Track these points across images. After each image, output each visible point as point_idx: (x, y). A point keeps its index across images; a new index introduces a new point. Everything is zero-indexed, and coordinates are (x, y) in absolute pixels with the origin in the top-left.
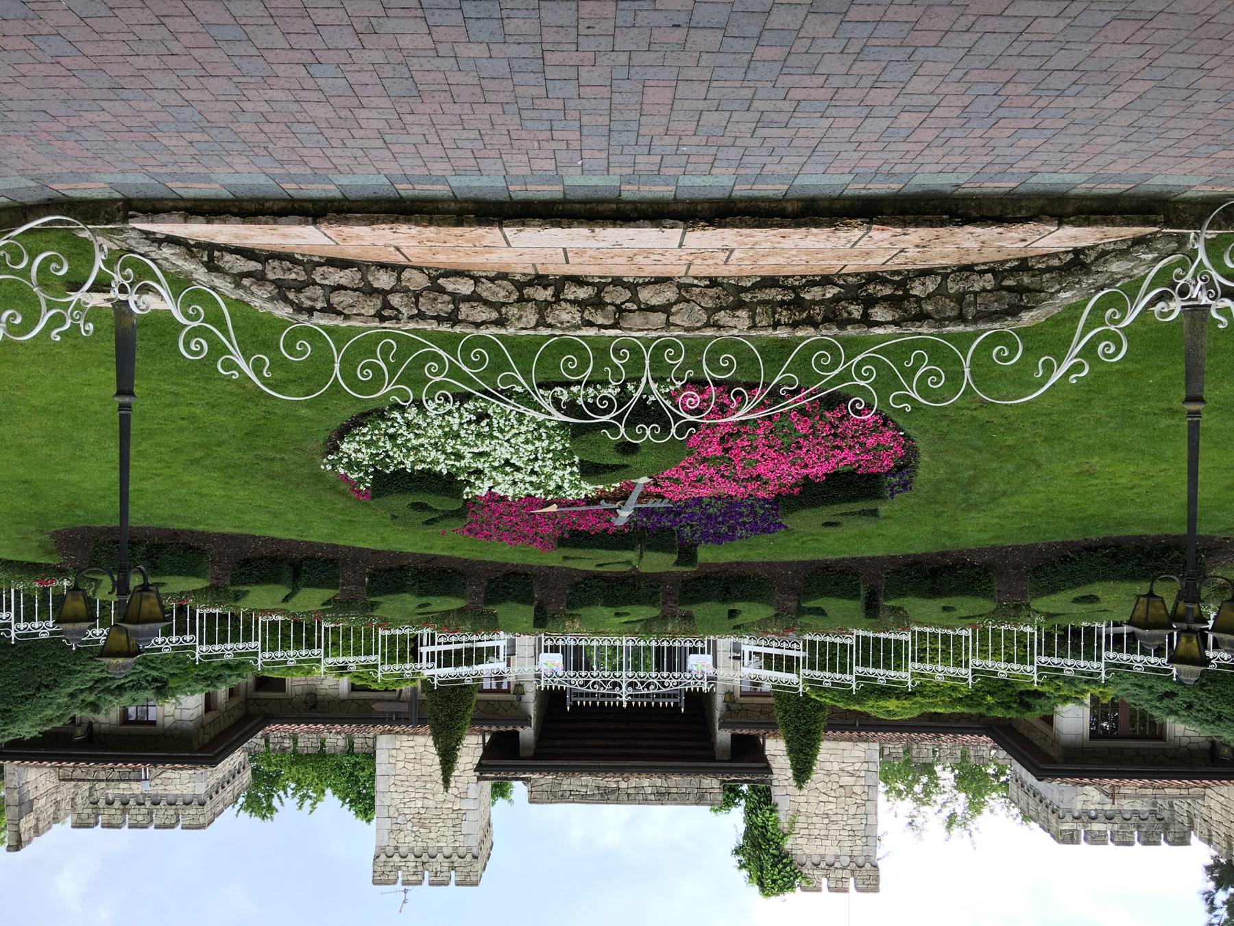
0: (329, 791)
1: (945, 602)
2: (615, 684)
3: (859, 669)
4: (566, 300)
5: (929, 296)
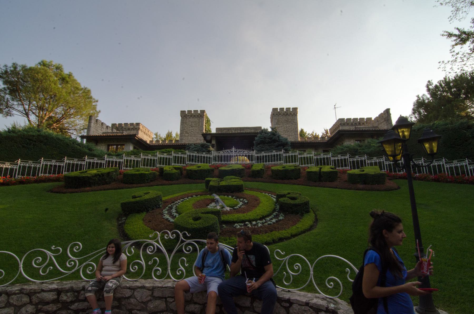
0: (270, 130)
1: (200, 168)
2: (236, 152)
3: (185, 156)
4: (199, 304)
5: (25, 305)
